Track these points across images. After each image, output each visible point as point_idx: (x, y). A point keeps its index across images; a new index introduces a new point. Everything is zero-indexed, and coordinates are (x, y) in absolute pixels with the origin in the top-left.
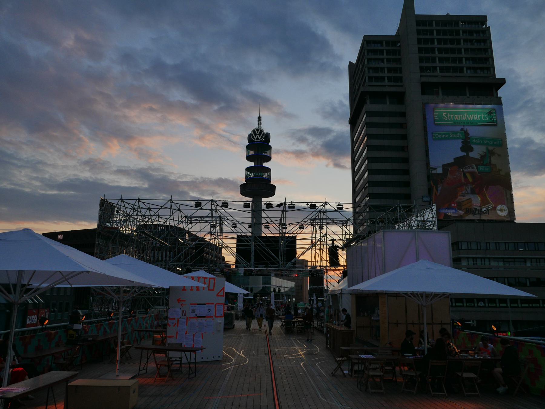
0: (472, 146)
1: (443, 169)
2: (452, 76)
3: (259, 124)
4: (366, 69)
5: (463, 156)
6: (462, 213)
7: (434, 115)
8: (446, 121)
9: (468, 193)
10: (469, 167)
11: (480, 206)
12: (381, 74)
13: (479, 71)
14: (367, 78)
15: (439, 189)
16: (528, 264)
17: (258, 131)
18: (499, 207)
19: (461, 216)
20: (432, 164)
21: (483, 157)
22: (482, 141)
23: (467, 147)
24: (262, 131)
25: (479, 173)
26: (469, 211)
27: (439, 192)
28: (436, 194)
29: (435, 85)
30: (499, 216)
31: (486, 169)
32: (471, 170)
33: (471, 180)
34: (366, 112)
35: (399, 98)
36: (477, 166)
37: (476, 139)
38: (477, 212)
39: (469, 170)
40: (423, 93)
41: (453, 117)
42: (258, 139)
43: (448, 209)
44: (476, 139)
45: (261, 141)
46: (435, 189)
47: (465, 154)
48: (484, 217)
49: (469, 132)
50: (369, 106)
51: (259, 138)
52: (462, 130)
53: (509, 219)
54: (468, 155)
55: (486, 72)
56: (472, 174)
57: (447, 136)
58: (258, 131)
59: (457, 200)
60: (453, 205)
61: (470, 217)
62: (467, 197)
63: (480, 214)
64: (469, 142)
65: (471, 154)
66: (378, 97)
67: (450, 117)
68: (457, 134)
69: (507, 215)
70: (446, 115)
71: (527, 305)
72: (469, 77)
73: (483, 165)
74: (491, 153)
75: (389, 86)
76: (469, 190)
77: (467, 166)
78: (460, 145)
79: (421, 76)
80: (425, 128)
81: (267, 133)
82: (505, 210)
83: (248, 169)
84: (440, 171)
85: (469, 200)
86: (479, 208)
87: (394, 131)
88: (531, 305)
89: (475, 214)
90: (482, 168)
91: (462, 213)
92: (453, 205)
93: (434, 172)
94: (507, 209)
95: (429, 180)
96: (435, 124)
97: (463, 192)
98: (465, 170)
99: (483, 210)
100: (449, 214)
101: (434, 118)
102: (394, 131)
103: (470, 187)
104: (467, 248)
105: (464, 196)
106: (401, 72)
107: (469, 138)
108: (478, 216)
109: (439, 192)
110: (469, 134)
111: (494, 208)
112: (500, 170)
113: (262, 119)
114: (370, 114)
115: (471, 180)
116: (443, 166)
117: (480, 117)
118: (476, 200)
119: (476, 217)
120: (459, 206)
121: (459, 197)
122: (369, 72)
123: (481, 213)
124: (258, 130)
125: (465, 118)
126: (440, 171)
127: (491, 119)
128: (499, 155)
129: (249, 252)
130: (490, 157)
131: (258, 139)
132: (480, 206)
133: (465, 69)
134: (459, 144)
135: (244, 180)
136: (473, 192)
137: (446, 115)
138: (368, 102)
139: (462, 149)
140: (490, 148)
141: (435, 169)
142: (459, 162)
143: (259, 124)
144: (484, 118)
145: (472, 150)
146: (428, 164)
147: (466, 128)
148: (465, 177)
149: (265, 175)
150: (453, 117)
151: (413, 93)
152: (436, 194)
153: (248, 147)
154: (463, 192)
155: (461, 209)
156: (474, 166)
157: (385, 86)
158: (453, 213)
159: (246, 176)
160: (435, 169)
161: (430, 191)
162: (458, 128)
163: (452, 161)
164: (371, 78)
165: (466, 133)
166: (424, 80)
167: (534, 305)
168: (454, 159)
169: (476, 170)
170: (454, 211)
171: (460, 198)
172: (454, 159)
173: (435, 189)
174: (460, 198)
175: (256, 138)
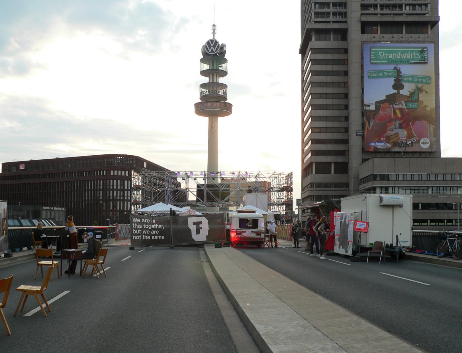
0: (404, 84)
1: (376, 106)
2: (390, 14)
3: (214, 33)
4: (313, 4)
5: (395, 93)
6: (389, 145)
7: (371, 54)
8: (381, 60)
9: (396, 128)
10: (399, 103)
11: (406, 140)
12: (326, 10)
13: (417, 7)
14: (313, 13)
15: (371, 124)
16: (430, 192)
17: (212, 43)
18: (422, 140)
19: (389, 149)
20: (366, 101)
21: (412, 94)
22: (412, 79)
23: (398, 85)
24: (216, 42)
25: (407, 109)
26: (395, 144)
27: (371, 127)
28: (368, 129)
29: (375, 24)
30: (422, 148)
31: (413, 106)
32: (400, 106)
33: (399, 115)
34: (311, 49)
35: (343, 34)
36: (406, 102)
37: (408, 77)
38: (403, 145)
39: (398, 106)
40: (363, 32)
41: (388, 56)
42: (212, 51)
43: (378, 142)
44: (408, 77)
45: (216, 54)
46: (367, 125)
47: (396, 91)
48: (409, 150)
49: (402, 70)
50: (314, 43)
51: (214, 51)
52: (395, 68)
53: (430, 151)
54: (399, 92)
55: (423, 7)
56: (401, 110)
57: (381, 74)
58: (212, 43)
59: (386, 134)
60: (382, 139)
61: (397, 149)
62: (395, 132)
63: (406, 147)
64: (401, 80)
65: (402, 92)
66: (322, 33)
67: (385, 56)
68: (390, 72)
69: (429, 147)
70: (382, 54)
71: (434, 224)
72: (407, 14)
73: (411, 101)
74: (420, 90)
75: (334, 22)
76: (397, 125)
77: (397, 103)
78: (393, 83)
79: (362, 14)
80: (362, 66)
81: (222, 44)
82: (427, 143)
83: (203, 86)
84: (373, 107)
85: (397, 134)
86: (405, 142)
87: (336, 68)
88: (437, 224)
89: (400, 147)
90: (410, 105)
91: (389, 145)
92: (382, 139)
93: (367, 108)
94: (429, 142)
95: (363, 116)
96: (371, 63)
97: (392, 127)
98: (395, 107)
99: (408, 143)
100: (378, 147)
101: (371, 57)
102: (336, 68)
103: (398, 122)
104: (423, 175)
105: (392, 131)
106: (345, 8)
107: (401, 76)
108: (404, 148)
109: (371, 127)
110: (401, 73)
111: (418, 142)
112: (426, 106)
113: (216, 28)
114: (315, 51)
115: (399, 115)
116: (376, 103)
117: (413, 56)
118: (403, 134)
119: (402, 150)
120: (388, 139)
121: (389, 132)
122: (315, 8)
123: (406, 145)
124: (212, 41)
125: (399, 57)
126: (373, 107)
127: (422, 57)
128: (427, 92)
129: (203, 193)
130: (418, 94)
131: (212, 51)
132: (406, 140)
133: (404, 6)
134: (391, 81)
135: (199, 97)
136: (401, 127)
137: (382, 54)
138: (313, 38)
139: (395, 87)
140: (419, 85)
141: (368, 106)
142: (391, 99)
143: (214, 33)
144: (416, 56)
145: (402, 87)
146: (363, 101)
147: (399, 66)
148: (395, 112)
149: (221, 93)
150: (388, 56)
151: (354, 32)
152: (368, 129)
153: (202, 61)
154: (392, 127)
155: (389, 143)
156: (403, 102)
157: (329, 22)
158: (382, 146)
159: (201, 93)
160: (368, 106)
161: (363, 126)
162: (392, 67)
163: (384, 98)
164: (316, 14)
165: (399, 72)
166: (365, 19)
167: (423, 224)
168: (386, 96)
169: (404, 107)
170: (383, 144)
171: (389, 133)
172: (386, 96)
173: (367, 125)
174: (389, 133)
175: (210, 51)
